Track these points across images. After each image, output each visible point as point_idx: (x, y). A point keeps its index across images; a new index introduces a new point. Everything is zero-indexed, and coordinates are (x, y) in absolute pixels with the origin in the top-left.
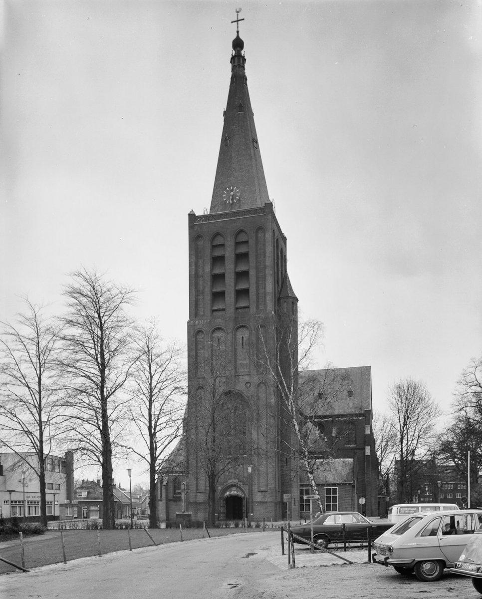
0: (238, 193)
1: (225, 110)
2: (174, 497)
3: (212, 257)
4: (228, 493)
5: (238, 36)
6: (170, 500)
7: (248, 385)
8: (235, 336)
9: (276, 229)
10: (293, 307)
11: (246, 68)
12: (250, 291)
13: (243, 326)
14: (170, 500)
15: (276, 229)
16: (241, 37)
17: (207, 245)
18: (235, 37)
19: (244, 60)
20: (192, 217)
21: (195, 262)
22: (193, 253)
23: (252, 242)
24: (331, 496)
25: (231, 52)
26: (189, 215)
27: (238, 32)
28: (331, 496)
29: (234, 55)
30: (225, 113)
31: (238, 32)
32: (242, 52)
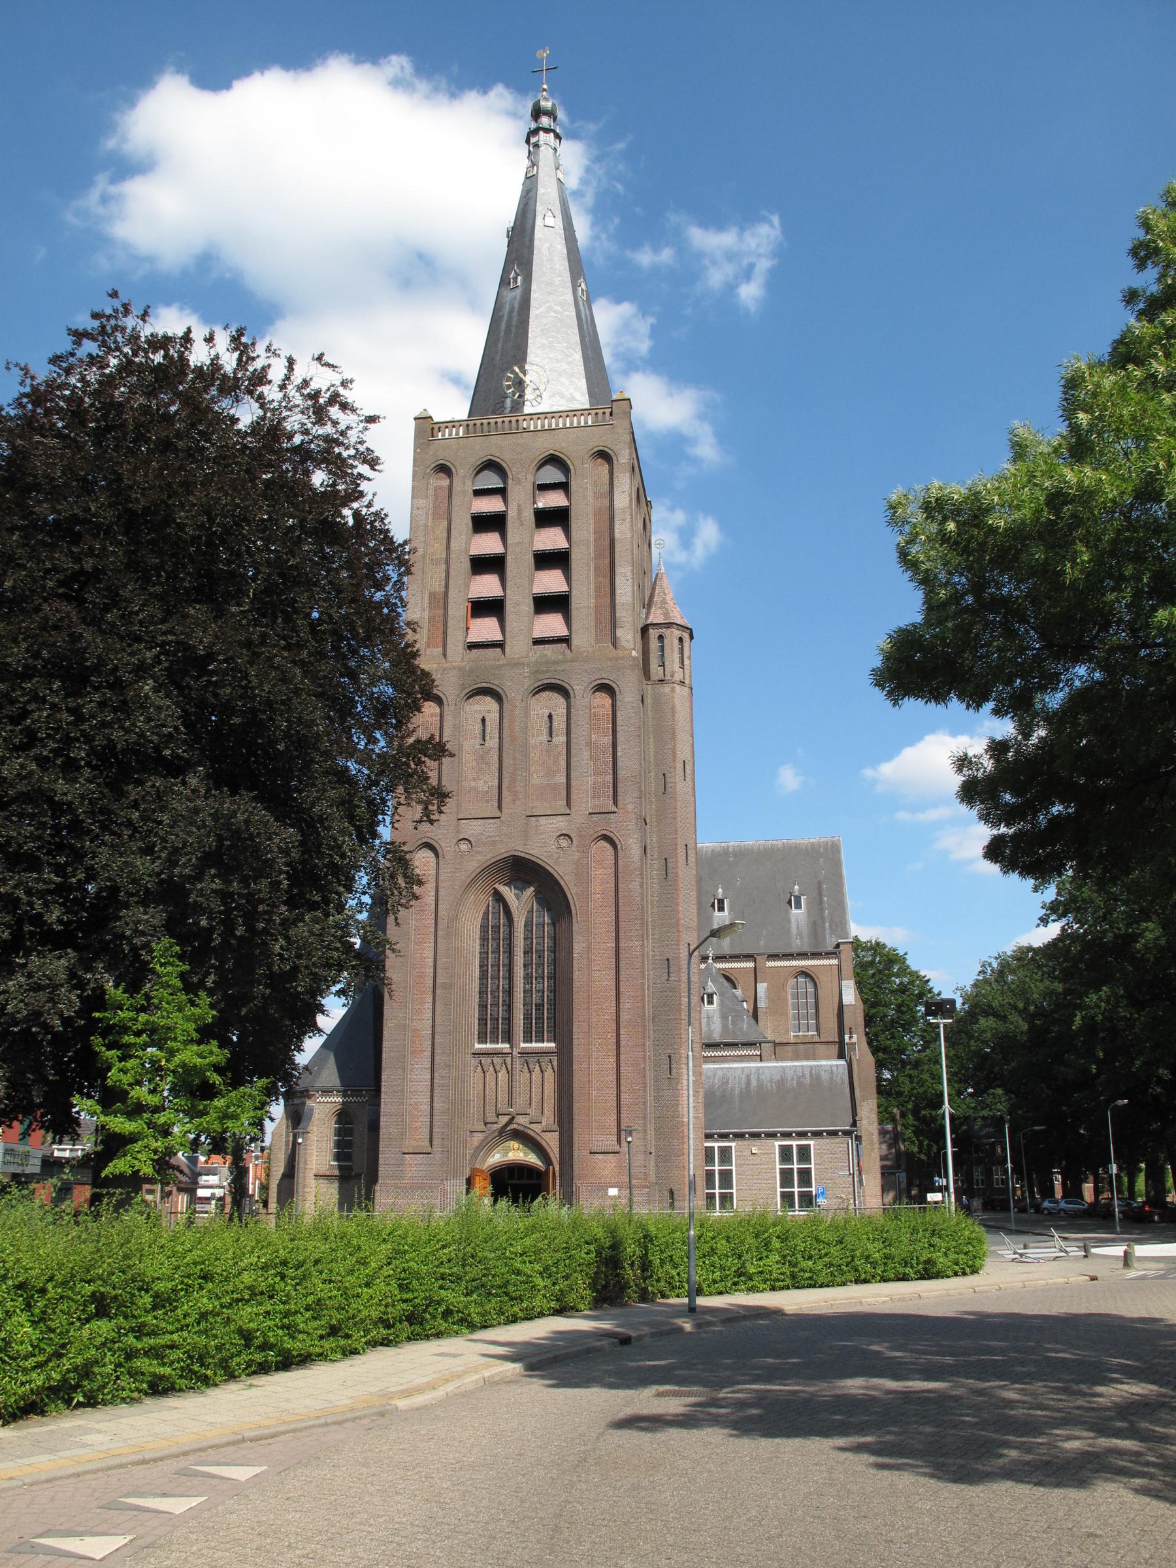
8: (526, 710)
24: (796, 1190)
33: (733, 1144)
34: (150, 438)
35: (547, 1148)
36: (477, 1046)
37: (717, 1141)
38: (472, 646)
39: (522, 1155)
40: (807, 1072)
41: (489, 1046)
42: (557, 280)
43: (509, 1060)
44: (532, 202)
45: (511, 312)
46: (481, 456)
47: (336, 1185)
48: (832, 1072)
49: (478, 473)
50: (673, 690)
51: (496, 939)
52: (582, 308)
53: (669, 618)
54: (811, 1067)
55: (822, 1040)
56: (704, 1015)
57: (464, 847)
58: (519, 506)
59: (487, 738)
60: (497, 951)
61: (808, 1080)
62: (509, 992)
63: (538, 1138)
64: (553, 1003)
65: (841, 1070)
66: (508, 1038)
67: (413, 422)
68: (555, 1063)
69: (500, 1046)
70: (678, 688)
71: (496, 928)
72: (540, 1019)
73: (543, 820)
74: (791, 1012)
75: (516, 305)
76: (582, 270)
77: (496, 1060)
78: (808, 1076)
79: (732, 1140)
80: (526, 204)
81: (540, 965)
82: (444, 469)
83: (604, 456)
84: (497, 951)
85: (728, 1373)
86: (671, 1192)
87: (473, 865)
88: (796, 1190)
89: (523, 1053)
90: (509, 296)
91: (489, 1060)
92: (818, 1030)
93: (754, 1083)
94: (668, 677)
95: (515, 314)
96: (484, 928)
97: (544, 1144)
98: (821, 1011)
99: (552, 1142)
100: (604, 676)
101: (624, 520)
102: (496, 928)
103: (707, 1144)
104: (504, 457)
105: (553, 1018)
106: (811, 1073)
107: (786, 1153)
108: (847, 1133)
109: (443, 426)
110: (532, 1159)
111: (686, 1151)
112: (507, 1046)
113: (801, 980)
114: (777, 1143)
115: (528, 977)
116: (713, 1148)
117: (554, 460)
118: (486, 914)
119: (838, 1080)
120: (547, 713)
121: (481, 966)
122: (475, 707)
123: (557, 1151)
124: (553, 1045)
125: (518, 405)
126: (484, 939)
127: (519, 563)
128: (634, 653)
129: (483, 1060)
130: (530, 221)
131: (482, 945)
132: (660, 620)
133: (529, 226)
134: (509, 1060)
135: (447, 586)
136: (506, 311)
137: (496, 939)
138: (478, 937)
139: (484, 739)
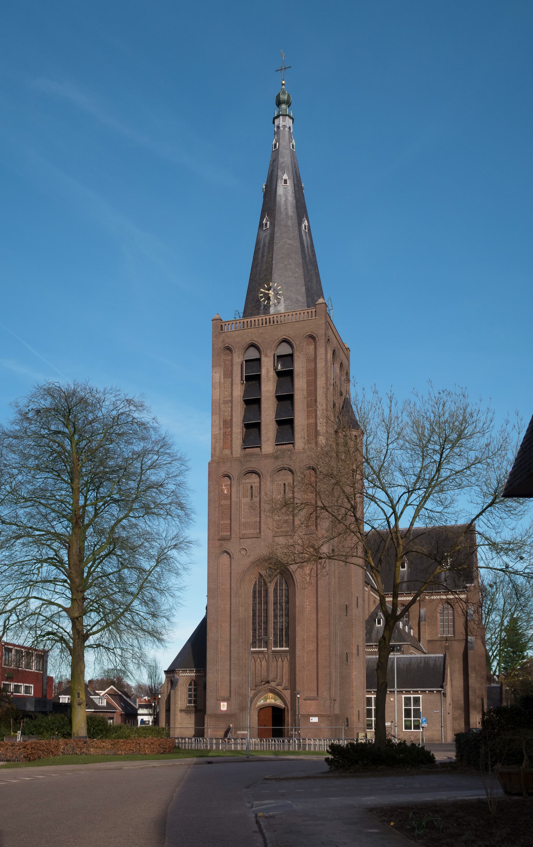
4: (262, 701)
33: (421, 696)
35: (286, 699)
36: (252, 649)
39: (273, 701)
40: (423, 661)
41: (257, 649)
42: (290, 223)
43: (266, 656)
44: (275, 169)
45: (264, 246)
46: (248, 341)
47: (193, 716)
48: (436, 661)
49: (245, 352)
51: (260, 597)
52: (304, 238)
54: (425, 657)
55: (456, 638)
56: (375, 629)
57: (243, 552)
59: (253, 497)
60: (260, 603)
61: (423, 664)
62: (266, 623)
63: (281, 693)
64: (287, 628)
65: (440, 659)
66: (266, 645)
68: (289, 657)
69: (262, 649)
71: (260, 593)
72: (281, 635)
74: (440, 624)
75: (267, 241)
76: (306, 212)
78: (423, 662)
79: (420, 694)
80: (272, 171)
81: (281, 609)
82: (229, 349)
83: (312, 337)
84: (260, 603)
86: (347, 719)
87: (247, 561)
88: (412, 719)
89: (274, 652)
90: (263, 235)
92: (454, 634)
95: (266, 248)
96: (254, 592)
97: (283, 696)
98: (456, 624)
99: (287, 694)
102: (260, 593)
103: (367, 696)
104: (258, 341)
105: (287, 635)
106: (425, 661)
107: (408, 700)
110: (279, 703)
112: (266, 649)
113: (446, 605)
114: (403, 696)
115: (275, 616)
116: (414, 729)
117: (285, 341)
118: (255, 585)
119: (438, 664)
121: (253, 611)
122: (247, 481)
123: (289, 699)
124: (288, 649)
125: (267, 308)
126: (254, 597)
130: (275, 183)
131: (253, 600)
133: (274, 187)
134: (266, 656)
135: (232, 416)
136: (262, 245)
137: (260, 597)
138: (251, 596)
139: (252, 497)
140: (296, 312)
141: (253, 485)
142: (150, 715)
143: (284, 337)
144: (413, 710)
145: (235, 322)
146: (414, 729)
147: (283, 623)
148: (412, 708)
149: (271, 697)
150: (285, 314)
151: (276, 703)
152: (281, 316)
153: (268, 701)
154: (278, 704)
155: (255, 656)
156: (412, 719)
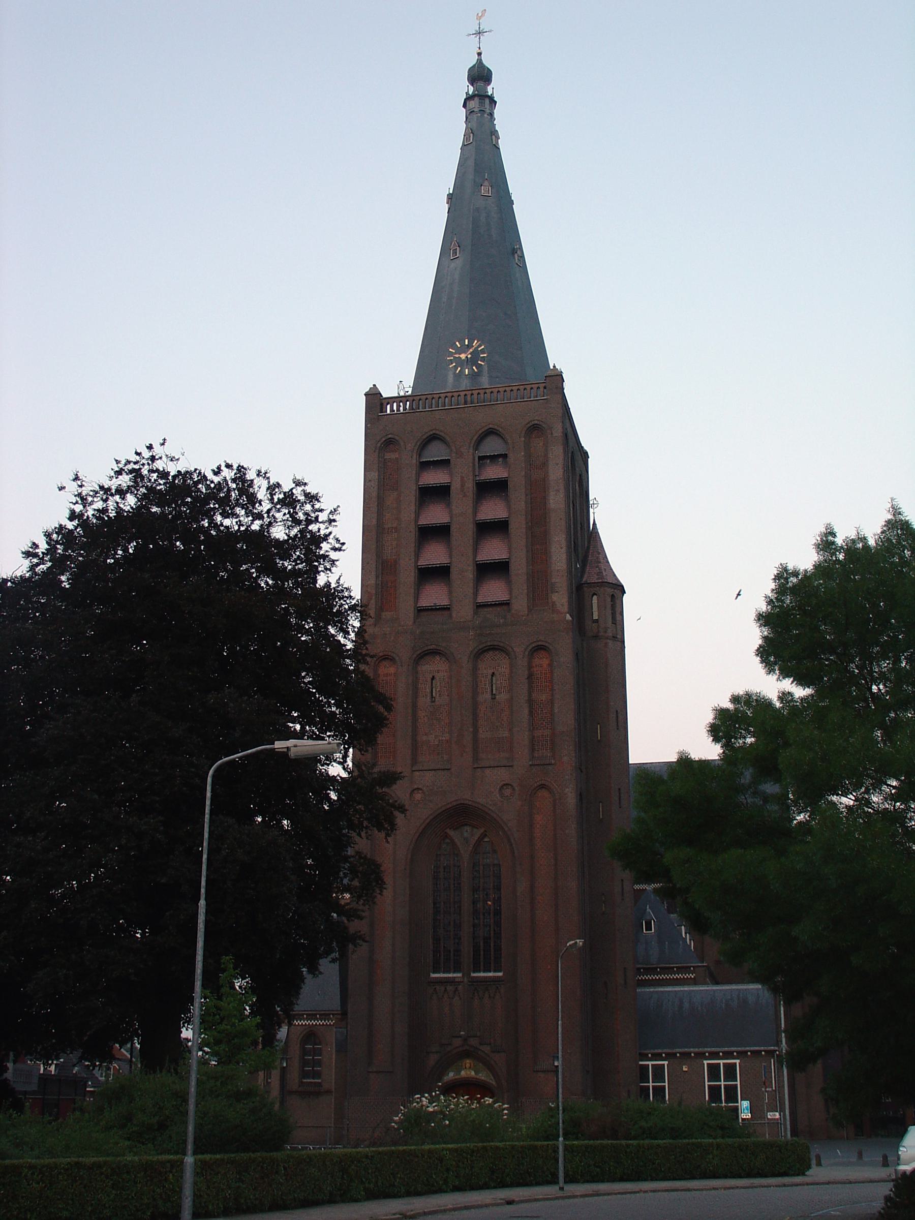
0: (483, 351)
1: (451, 192)
2: (302, 1084)
3: (419, 569)
4: (451, 1074)
5: (480, 62)
6: (291, 1092)
7: (507, 792)
8: (475, 669)
9: (569, 430)
10: (613, 607)
11: (495, 116)
12: (513, 567)
13: (493, 648)
14: (291, 1092)
15: (569, 430)
16: (486, 62)
17: (408, 458)
18: (473, 61)
19: (493, 102)
20: (374, 400)
21: (379, 497)
22: (374, 475)
23: (517, 457)
24: (651, 1084)
25: (464, 88)
26: (365, 395)
27: (479, 54)
28: (651, 1084)
29: (470, 93)
30: (450, 197)
31: (479, 54)
32: (489, 89)
34: (246, 578)
37: (650, 1060)
38: (420, 611)
39: (473, 1073)
50: (606, 645)
53: (602, 578)
58: (462, 478)
67: (364, 397)
70: (610, 643)
73: (488, 771)
75: (457, 276)
77: (450, 988)
85: (454, 450)
91: (443, 988)
93: (686, 1005)
94: (601, 634)
100: (541, 638)
101: (558, 491)
107: (713, 1070)
108: (554, 1071)
109: (390, 401)
111: (776, 1063)
114: (705, 1062)
116: (720, 1064)
120: (490, 672)
127: (463, 534)
128: (568, 617)
129: (438, 988)
132: (594, 579)
140: (526, 386)
141: (436, 674)
142: (344, 906)
143: (491, 426)
144: (724, 1066)
145: (457, 394)
146: (720, 1064)
147: (490, 927)
148: (723, 1083)
149: (468, 1065)
150: (500, 389)
151: (478, 1077)
152: (459, 396)
153: (463, 1073)
154: (483, 1078)
155: (438, 988)
156: (723, 1083)
